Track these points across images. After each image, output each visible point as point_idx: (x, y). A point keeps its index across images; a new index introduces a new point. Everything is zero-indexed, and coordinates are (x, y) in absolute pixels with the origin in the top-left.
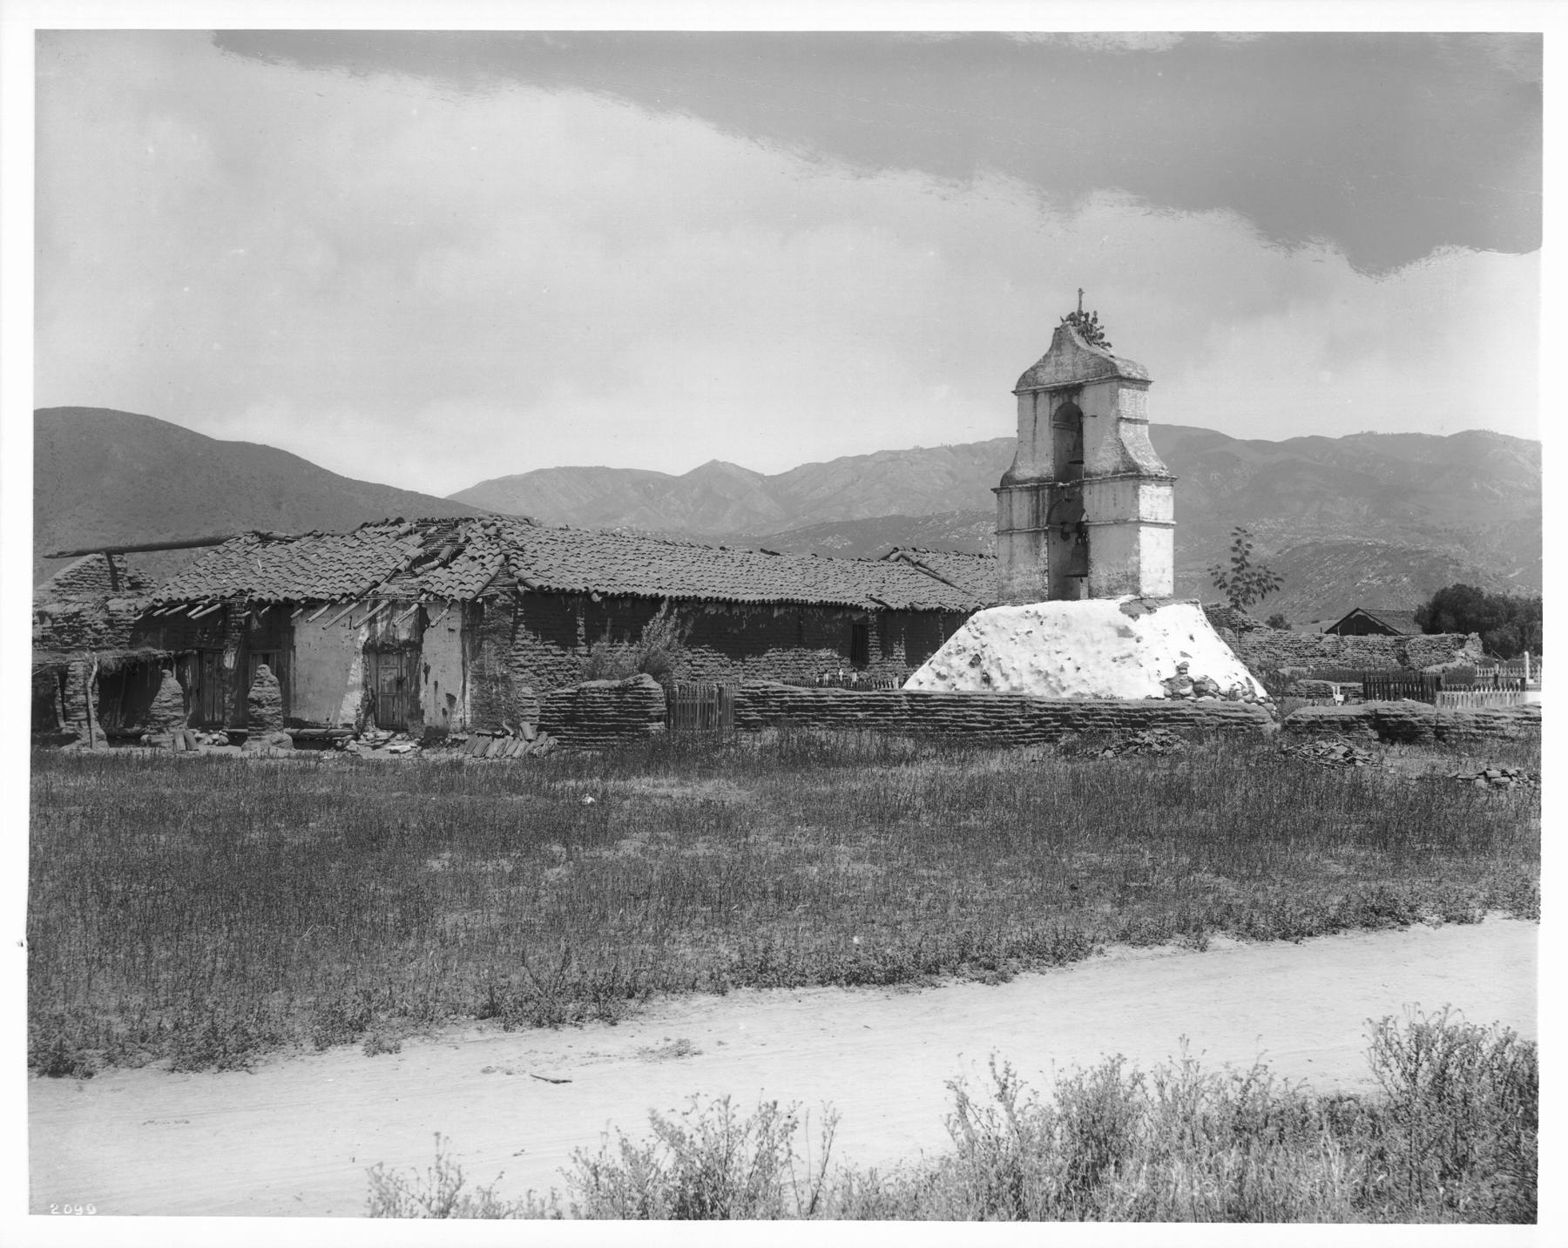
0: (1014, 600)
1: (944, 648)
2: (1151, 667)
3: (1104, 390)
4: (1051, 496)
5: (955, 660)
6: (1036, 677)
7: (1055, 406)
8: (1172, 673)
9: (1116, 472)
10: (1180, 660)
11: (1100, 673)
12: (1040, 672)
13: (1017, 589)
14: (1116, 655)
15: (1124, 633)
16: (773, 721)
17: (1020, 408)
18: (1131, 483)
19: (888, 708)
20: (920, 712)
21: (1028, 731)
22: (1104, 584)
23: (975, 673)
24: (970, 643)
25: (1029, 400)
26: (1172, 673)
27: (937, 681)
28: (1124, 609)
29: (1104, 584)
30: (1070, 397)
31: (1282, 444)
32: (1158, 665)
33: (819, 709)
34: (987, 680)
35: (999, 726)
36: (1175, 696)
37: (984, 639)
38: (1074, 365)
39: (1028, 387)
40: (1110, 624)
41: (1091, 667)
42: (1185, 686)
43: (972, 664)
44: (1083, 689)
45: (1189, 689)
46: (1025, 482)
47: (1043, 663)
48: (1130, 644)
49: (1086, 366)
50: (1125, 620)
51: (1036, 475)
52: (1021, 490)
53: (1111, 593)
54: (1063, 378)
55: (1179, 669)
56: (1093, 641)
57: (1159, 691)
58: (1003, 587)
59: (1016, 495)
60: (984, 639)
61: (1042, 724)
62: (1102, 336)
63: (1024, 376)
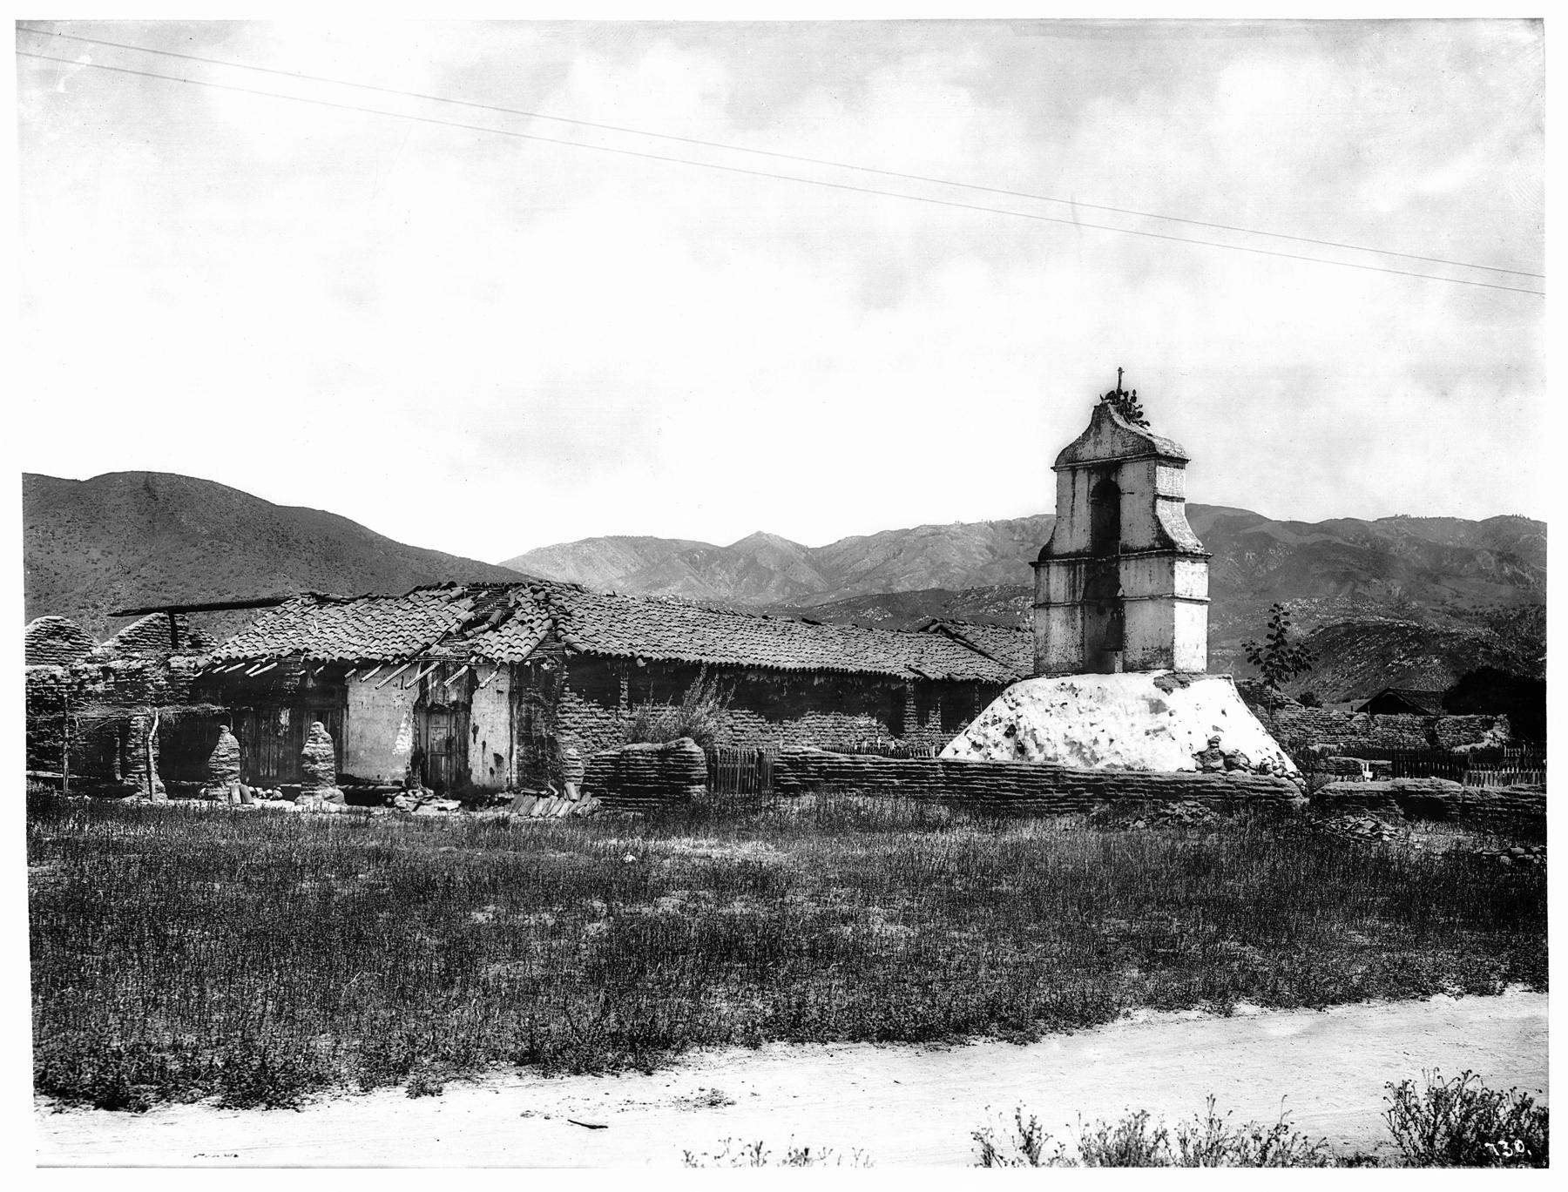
1: (980, 719)
7: (1094, 482)
8: (1204, 746)
10: (1212, 734)
18: (1166, 559)
20: (956, 781)
26: (1204, 746)
32: (1190, 739)
33: (854, 775)
34: (1021, 749)
40: (1144, 698)
42: (1215, 758)
43: (1007, 735)
45: (1220, 763)
48: (1163, 718)
50: (1158, 694)
53: (1144, 668)
55: (1210, 742)
57: (1191, 764)
59: (1053, 569)
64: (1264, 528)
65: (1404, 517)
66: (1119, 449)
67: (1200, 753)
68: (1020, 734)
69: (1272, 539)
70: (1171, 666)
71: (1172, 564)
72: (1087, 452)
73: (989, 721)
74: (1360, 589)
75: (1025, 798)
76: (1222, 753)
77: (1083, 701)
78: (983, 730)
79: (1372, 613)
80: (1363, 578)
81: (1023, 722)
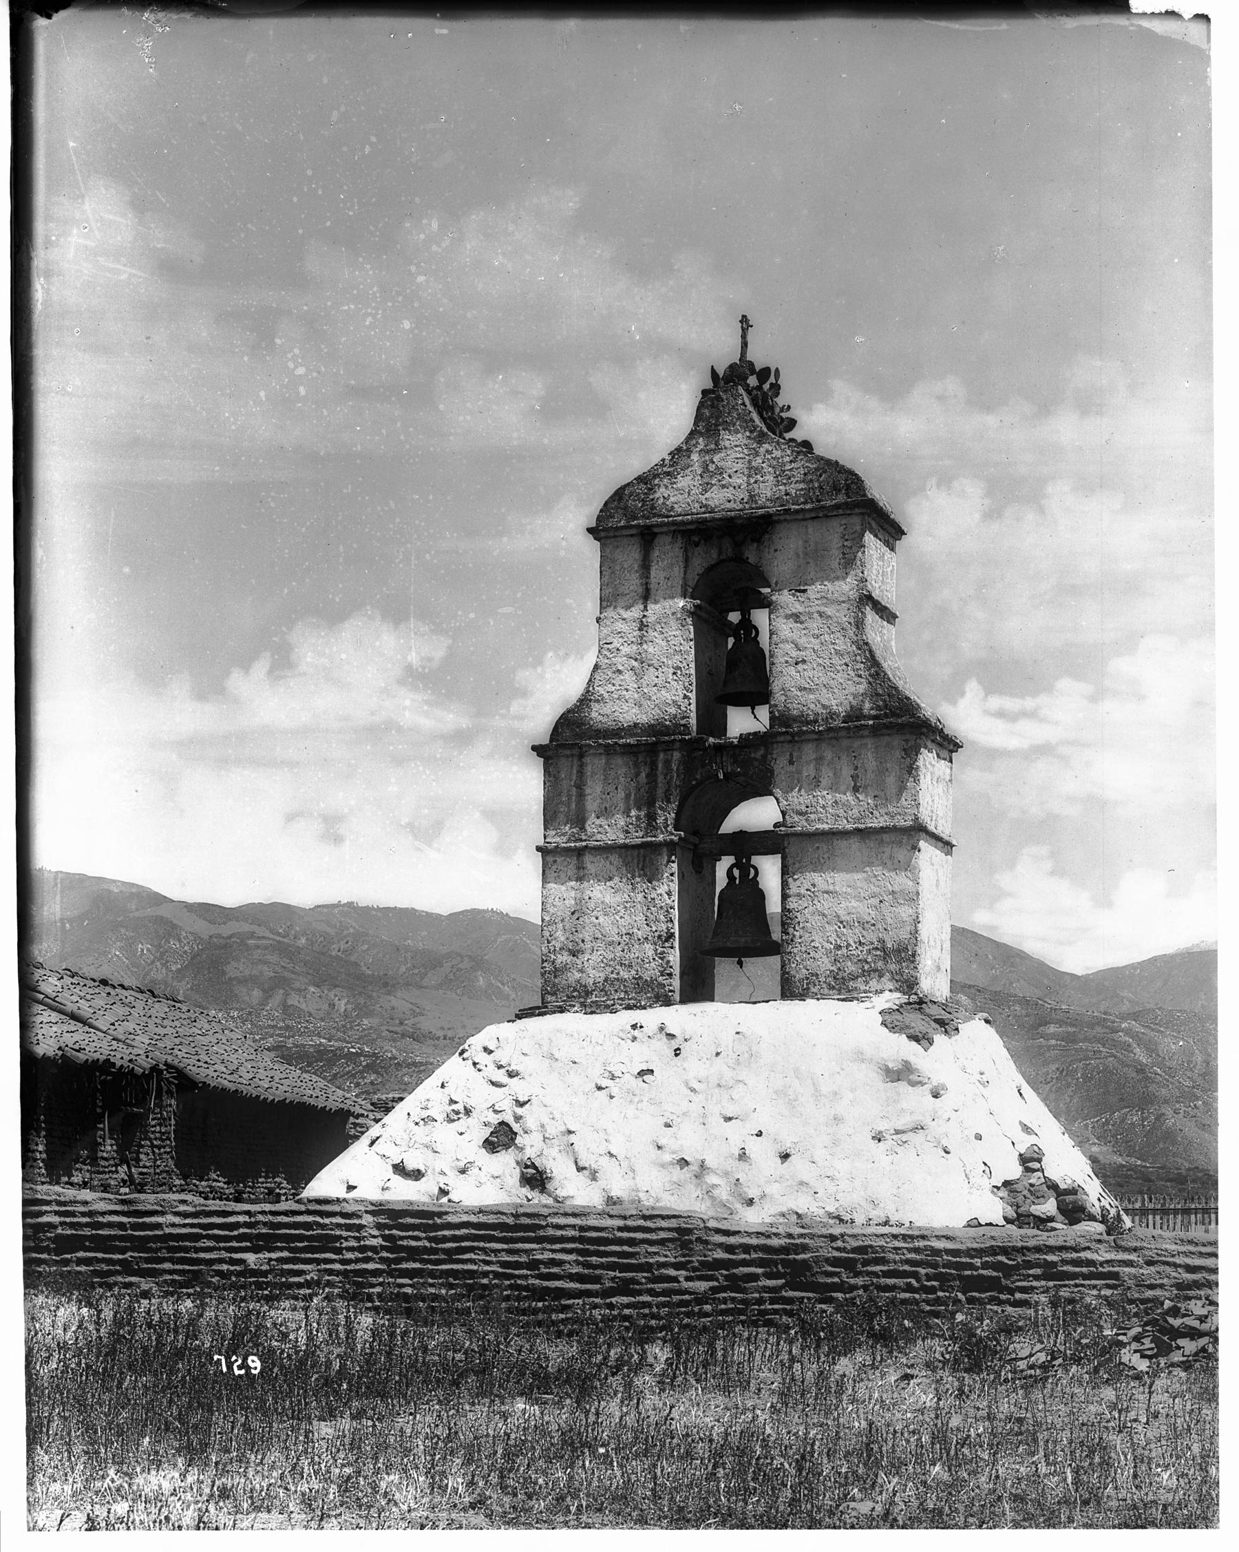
0: (589, 999)
1: (411, 1104)
2: (976, 1155)
3: (832, 534)
4: (688, 766)
5: (444, 1134)
6: (677, 1174)
7: (699, 563)
8: (1014, 1171)
9: (855, 715)
10: (1024, 1143)
11: (842, 1167)
12: (684, 1163)
13: (594, 975)
14: (882, 1126)
15: (902, 1074)
16: (554, 1323)
17: (606, 563)
18: (897, 741)
19: (327, 1243)
20: (413, 1254)
21: (701, 1299)
22: (824, 965)
23: (505, 1163)
24: (481, 1096)
25: (630, 555)
26: (1014, 1171)
27: (397, 1180)
28: (891, 1021)
29: (824, 965)
30: (738, 545)
31: (239, 909)
32: (981, 1152)
33: (140, 1244)
34: (535, 1178)
35: (624, 1288)
36: (1020, 1219)
37: (518, 1088)
38: (753, 470)
39: (630, 526)
40: (860, 1057)
41: (820, 1154)
42: (1038, 1196)
43: (491, 1146)
44: (803, 1203)
45: (1049, 1207)
46: (618, 732)
47: (689, 1141)
48: (915, 1101)
49: (782, 475)
50: (899, 1047)
51: (643, 719)
52: (609, 751)
53: (843, 987)
54: (722, 499)
55: (1024, 1160)
56: (817, 1095)
57: (993, 1210)
58: (557, 972)
59: (594, 764)
60: (518, 1088)
61: (735, 1283)
62: (792, 423)
63: (619, 495)
64: (163, 911)
65: (350, 904)
66: (767, 489)
67: (1007, 1184)
68: (530, 1145)
69: (174, 926)
70: (908, 985)
71: (911, 753)
72: (683, 496)
73: (438, 1110)
74: (294, 1000)
75: (606, 1294)
76: (1053, 1186)
77: (694, 1066)
78: (421, 1133)
79: (311, 1034)
80: (297, 985)
81: (532, 1117)
